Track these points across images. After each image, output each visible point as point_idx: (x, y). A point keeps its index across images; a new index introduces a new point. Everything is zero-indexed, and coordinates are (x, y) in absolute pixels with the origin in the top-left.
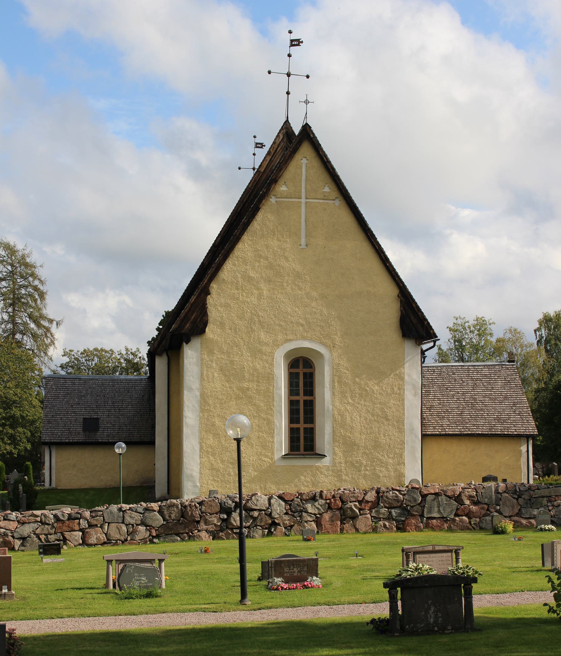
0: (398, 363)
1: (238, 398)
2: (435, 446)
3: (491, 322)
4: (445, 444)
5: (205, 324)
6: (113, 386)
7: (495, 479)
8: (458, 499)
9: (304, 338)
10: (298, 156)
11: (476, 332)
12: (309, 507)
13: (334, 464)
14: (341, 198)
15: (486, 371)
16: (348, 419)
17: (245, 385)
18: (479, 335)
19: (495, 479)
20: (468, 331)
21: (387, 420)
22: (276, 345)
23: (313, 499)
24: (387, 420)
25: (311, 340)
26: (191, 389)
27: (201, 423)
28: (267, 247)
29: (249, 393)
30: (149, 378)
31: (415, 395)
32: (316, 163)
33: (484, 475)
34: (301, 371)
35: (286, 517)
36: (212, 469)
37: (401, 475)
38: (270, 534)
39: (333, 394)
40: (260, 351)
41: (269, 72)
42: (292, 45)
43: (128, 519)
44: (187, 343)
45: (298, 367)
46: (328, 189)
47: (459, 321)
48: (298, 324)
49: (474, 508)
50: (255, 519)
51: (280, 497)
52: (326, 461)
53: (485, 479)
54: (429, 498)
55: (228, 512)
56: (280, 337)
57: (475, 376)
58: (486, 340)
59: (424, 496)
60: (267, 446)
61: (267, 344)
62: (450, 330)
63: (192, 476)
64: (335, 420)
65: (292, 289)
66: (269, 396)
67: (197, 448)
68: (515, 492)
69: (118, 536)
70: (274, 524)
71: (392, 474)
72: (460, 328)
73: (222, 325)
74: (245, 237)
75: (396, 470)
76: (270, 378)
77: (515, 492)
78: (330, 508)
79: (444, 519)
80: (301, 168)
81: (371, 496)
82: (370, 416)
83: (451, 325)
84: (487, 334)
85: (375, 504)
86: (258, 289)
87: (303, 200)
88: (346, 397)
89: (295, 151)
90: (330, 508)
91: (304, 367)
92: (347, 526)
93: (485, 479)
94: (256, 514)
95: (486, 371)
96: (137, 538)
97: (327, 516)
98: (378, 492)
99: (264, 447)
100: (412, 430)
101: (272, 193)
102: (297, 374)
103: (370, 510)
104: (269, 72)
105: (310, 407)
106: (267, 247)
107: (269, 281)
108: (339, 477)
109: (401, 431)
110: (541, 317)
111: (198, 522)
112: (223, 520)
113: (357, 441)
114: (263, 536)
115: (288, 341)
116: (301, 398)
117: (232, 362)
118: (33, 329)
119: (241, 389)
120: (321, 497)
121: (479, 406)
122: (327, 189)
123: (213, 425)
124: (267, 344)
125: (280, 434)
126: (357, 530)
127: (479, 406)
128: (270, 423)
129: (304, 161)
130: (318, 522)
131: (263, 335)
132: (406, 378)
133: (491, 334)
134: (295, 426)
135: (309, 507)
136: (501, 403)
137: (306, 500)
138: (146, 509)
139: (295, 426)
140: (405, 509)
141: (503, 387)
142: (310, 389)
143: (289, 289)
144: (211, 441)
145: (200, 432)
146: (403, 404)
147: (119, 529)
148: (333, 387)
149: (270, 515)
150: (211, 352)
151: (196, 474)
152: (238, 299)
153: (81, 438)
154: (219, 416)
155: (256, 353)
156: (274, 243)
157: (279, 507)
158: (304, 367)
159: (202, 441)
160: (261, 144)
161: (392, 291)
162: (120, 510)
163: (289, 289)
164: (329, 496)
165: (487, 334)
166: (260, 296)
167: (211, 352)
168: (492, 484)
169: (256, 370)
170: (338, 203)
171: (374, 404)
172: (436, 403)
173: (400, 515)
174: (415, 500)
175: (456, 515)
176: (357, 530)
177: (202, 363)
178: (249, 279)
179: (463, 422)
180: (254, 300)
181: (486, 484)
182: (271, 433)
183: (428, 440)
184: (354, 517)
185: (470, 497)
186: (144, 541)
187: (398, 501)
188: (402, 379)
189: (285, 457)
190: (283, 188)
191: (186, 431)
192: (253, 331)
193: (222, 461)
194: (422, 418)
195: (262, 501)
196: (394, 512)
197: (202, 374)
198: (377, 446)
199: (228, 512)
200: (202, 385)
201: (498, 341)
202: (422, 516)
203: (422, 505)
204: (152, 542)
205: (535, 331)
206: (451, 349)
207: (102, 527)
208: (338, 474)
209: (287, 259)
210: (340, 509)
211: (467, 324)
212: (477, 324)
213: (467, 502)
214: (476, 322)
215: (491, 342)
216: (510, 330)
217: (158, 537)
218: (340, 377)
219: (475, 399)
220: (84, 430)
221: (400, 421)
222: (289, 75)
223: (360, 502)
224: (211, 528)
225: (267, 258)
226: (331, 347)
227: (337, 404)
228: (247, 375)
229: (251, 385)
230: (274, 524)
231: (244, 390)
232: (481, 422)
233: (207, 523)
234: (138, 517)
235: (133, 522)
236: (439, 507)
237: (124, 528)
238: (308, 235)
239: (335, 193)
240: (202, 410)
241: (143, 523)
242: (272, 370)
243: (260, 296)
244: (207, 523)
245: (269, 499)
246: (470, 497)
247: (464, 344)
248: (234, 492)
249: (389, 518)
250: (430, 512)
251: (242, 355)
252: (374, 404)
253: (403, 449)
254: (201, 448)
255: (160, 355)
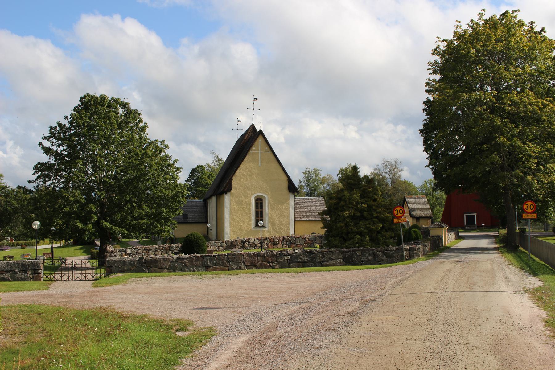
0: (287, 200)
1: (241, 210)
2: (299, 224)
3: (320, 170)
4: (301, 222)
5: (231, 188)
6: (192, 203)
7: (315, 234)
8: (305, 239)
9: (260, 192)
10: (258, 139)
11: (314, 174)
12: (265, 241)
13: (269, 230)
14: (271, 151)
15: (314, 200)
16: (273, 216)
17: (243, 206)
18: (316, 175)
19: (315, 234)
20: (311, 174)
21: (284, 216)
22: (252, 194)
23: (266, 239)
24: (284, 216)
25: (262, 193)
26: (227, 208)
27: (230, 218)
28: (249, 166)
29: (244, 209)
30: (258, 222)
31: (293, 209)
32: (263, 141)
33: (313, 232)
34: (259, 202)
35: (259, 244)
36: (233, 231)
37: (288, 233)
38: (255, 249)
39: (269, 209)
40: (247, 197)
41: (247, 108)
42: (254, 100)
43: (217, 245)
44: (226, 194)
45: (258, 201)
46: (267, 148)
47: (308, 170)
48: (258, 188)
49: (309, 241)
50: (251, 245)
51: (257, 239)
52: (267, 229)
53: (312, 234)
54: (297, 239)
55: (244, 243)
56: (253, 192)
57: (311, 201)
58: (319, 177)
59: (296, 238)
60: (249, 224)
61: (249, 194)
62: (304, 173)
63: (227, 233)
64: (269, 216)
65: (257, 178)
66: (250, 210)
67: (229, 225)
68: (320, 237)
69: (214, 249)
70: (256, 246)
71: (286, 232)
72: (308, 172)
73: (236, 189)
74: (243, 163)
75: (287, 231)
76: (250, 204)
77: (320, 237)
78: (270, 242)
79: (301, 244)
80: (259, 142)
81: (281, 238)
82: (279, 216)
83: (304, 172)
84: (319, 175)
85: (283, 241)
86: (247, 178)
87: (260, 152)
88: (272, 210)
89: (257, 137)
90: (270, 242)
91: (260, 201)
92: (275, 246)
93: (312, 234)
94: (251, 243)
95: (314, 200)
96: (220, 250)
97: (270, 244)
98: (283, 237)
99: (248, 224)
100: (292, 219)
101: (251, 150)
102: (258, 203)
103: (281, 242)
104: (247, 108)
105: (262, 213)
106: (249, 166)
107: (250, 176)
108: (271, 234)
109: (288, 220)
110: (340, 169)
111: (236, 246)
112: (242, 245)
113: (276, 223)
114: (253, 249)
115: (255, 193)
116: (259, 210)
117: (239, 200)
118: (333, 250)
119: (242, 208)
120: (268, 238)
121: (312, 211)
122: (267, 149)
123: (234, 218)
124: (249, 194)
125: (253, 221)
126: (278, 248)
127: (312, 211)
128: (250, 217)
129: (260, 140)
130: (267, 245)
131: (248, 192)
132: (290, 204)
133: (320, 175)
134: (257, 218)
135: (265, 241)
136: (319, 210)
137: (264, 240)
138: (222, 242)
139: (257, 218)
140: (291, 242)
141: (319, 205)
142: (262, 207)
143: (255, 178)
144: (233, 223)
145: (230, 220)
146: (289, 212)
147: (215, 248)
148: (268, 207)
149: (255, 244)
150: (233, 197)
151: (229, 233)
152: (240, 181)
153: (182, 221)
154: (235, 215)
155: (246, 197)
156: (251, 165)
157: (257, 242)
158: (260, 201)
159: (230, 223)
160: (256, 98)
161: (286, 178)
162: (215, 242)
163: (255, 178)
164: (270, 238)
165: (319, 175)
166: (247, 180)
167: (233, 197)
168: (314, 235)
169: (246, 202)
170: (270, 152)
171: (281, 212)
172: (298, 210)
173: (289, 243)
174: (293, 239)
175: (304, 243)
176: (278, 248)
177: (230, 200)
178: (244, 175)
179: (307, 216)
180: (245, 181)
181: (313, 235)
182: (250, 220)
183: (296, 222)
184: (277, 244)
185: (308, 238)
186: (221, 251)
187: (289, 239)
188: (289, 204)
189: (254, 227)
190: (254, 148)
191: (225, 220)
192: (245, 190)
193: (236, 229)
194: (295, 215)
195: (253, 240)
196: (288, 243)
197: (230, 203)
198: (281, 224)
199: (244, 243)
200: (230, 206)
201: (323, 177)
202: (295, 244)
203: (295, 241)
204: (223, 251)
205: (337, 175)
206: (304, 181)
207: (210, 247)
208: (270, 232)
209: (255, 169)
210: (273, 242)
211: (311, 171)
212: (315, 171)
213: (307, 240)
214: (314, 170)
215: (320, 178)
216: (327, 175)
217: (225, 249)
218: (270, 204)
219: (311, 209)
220: (183, 218)
221: (288, 217)
222: (253, 109)
223: (279, 240)
224: (239, 247)
225: (249, 169)
226: (268, 195)
227: (270, 212)
228: (243, 203)
229: (245, 207)
230: (256, 246)
231: (243, 208)
232: (313, 216)
233: (238, 246)
234: (220, 244)
235: (218, 245)
236: (300, 241)
237: (216, 247)
238: (261, 162)
239: (269, 150)
240: (230, 214)
241: (221, 246)
242: (251, 202)
243: (247, 180)
244: (238, 246)
245: (254, 239)
246: (308, 238)
247: (310, 179)
248: (260, 237)
249: (286, 244)
250: (297, 242)
251: (242, 198)
252: (281, 212)
253: (289, 225)
254: (230, 225)
255: (214, 196)
